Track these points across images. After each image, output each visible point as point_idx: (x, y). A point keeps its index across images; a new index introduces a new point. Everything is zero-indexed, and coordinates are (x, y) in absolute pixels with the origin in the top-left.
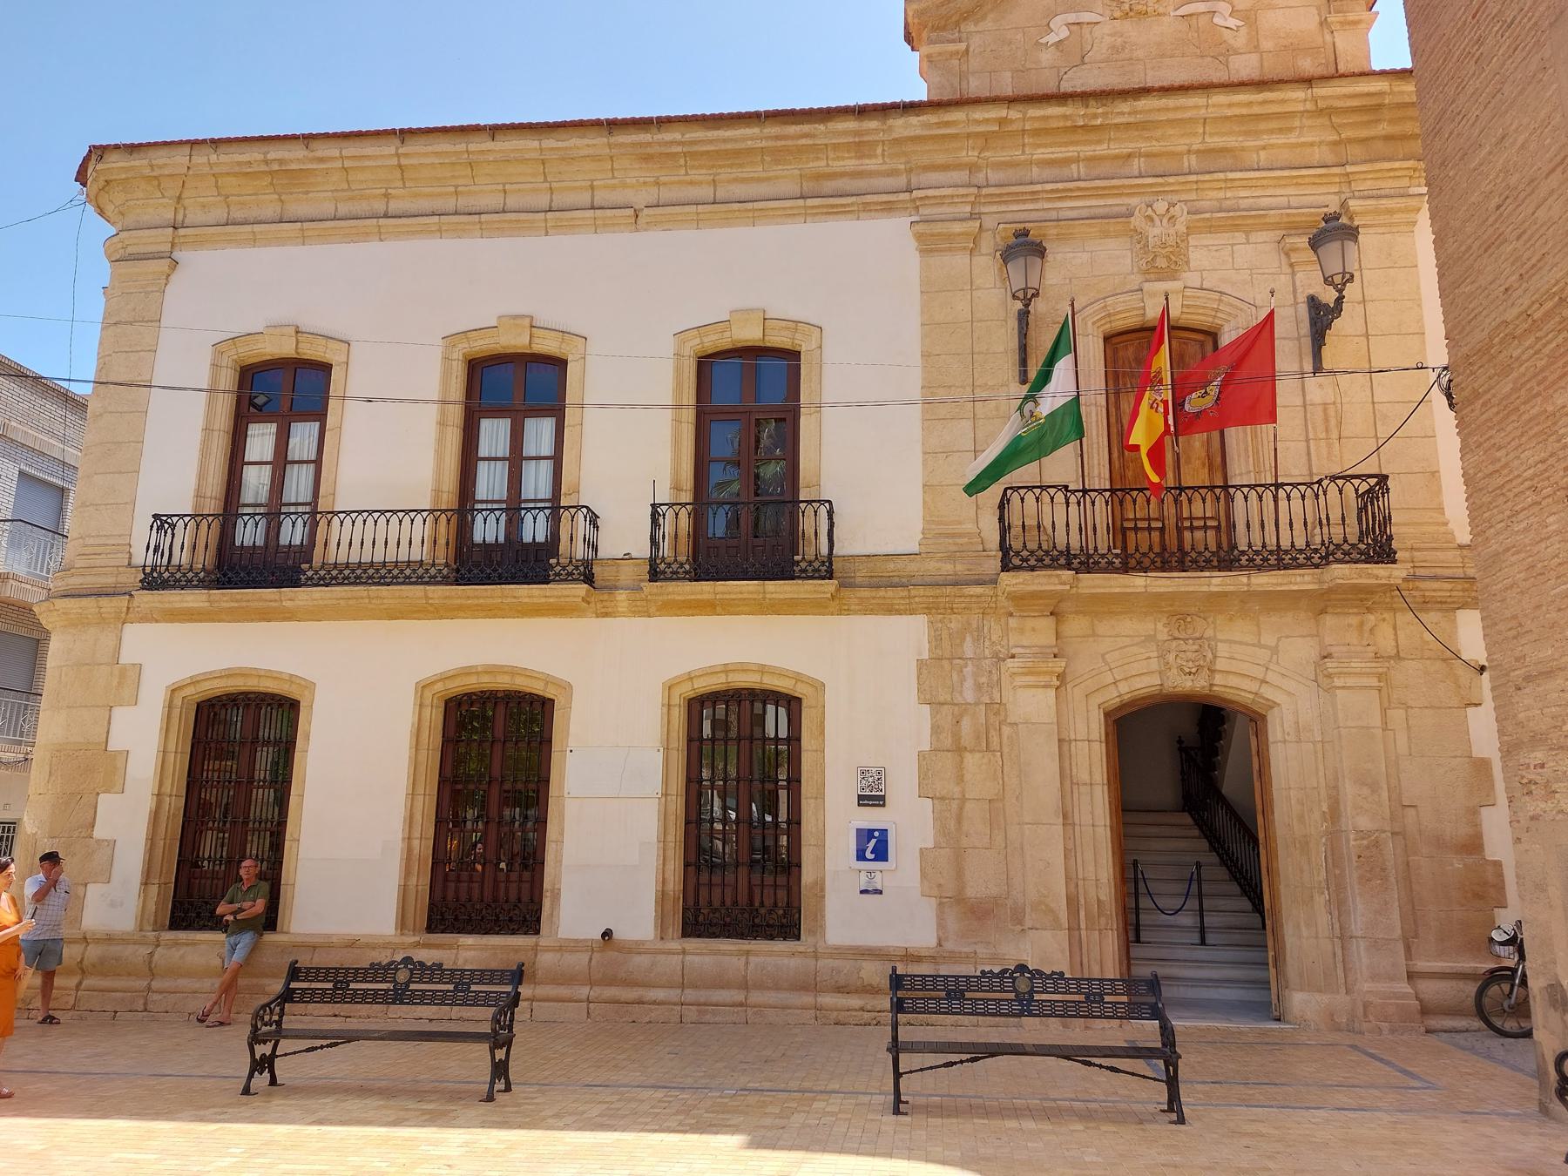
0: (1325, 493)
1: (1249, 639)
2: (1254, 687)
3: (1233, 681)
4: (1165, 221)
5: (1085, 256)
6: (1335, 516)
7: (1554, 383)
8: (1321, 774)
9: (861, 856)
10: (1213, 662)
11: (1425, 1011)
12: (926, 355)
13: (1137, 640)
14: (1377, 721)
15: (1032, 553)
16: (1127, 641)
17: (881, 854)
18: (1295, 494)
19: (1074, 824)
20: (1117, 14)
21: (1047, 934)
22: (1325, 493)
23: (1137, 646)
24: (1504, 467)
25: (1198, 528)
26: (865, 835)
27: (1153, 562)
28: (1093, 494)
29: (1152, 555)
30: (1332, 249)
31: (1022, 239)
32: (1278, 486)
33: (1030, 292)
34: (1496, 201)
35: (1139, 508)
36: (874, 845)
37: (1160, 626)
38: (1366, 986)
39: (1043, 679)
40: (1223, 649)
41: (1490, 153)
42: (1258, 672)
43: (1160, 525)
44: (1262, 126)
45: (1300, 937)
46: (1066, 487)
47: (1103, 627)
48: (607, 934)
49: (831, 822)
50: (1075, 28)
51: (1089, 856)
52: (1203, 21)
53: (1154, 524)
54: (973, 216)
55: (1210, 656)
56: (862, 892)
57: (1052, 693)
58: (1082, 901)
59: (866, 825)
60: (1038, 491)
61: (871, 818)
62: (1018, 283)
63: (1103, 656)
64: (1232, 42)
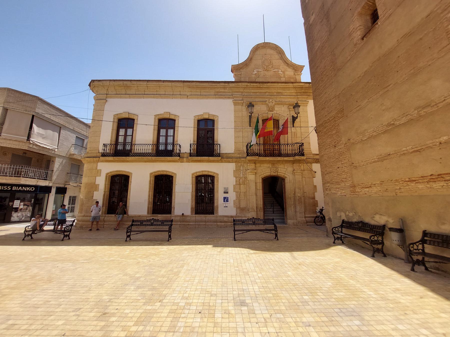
3: (281, 174)
6: (296, 149)
9: (224, 201)
11: (307, 222)
17: (227, 201)
36: (226, 199)
47: (262, 165)
48: (183, 214)
49: (219, 195)
61: (226, 195)
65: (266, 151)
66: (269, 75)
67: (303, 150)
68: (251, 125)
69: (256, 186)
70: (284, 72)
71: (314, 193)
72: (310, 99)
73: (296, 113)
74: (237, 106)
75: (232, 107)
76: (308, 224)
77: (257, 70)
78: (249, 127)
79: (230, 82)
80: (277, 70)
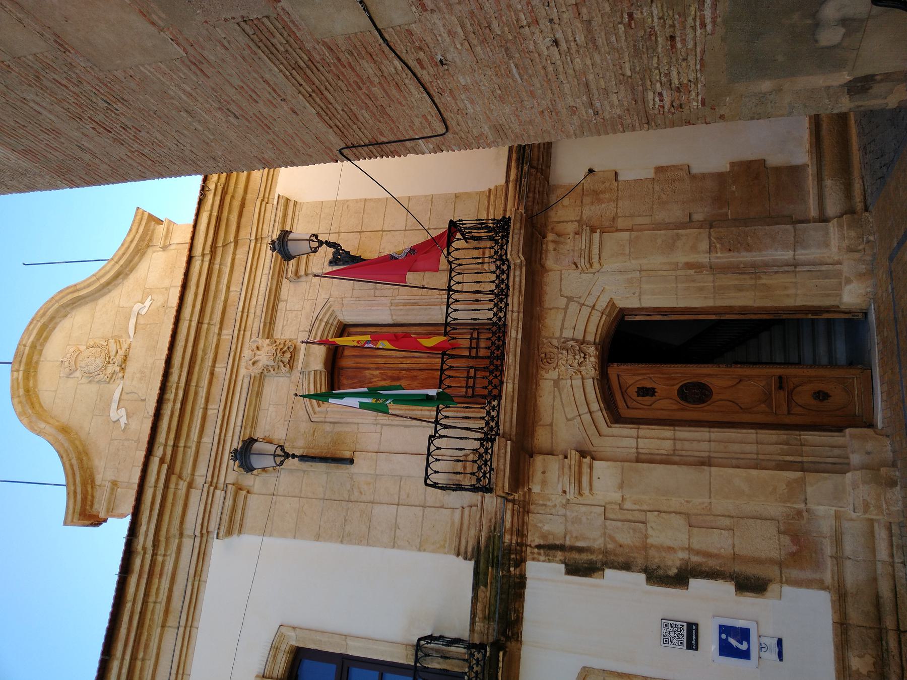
0: (458, 259)
1: (560, 317)
2: (596, 316)
3: (592, 328)
4: (258, 352)
5: (272, 409)
6: (476, 253)
7: (358, 75)
8: (665, 273)
9: (746, 655)
10: (577, 341)
11: (851, 211)
12: (318, 538)
13: (557, 394)
14: (626, 235)
15: (480, 468)
16: (558, 400)
17: (744, 634)
18: (458, 278)
19: (709, 457)
20: (121, 375)
21: (809, 490)
22: (458, 259)
23: (568, 398)
24: (426, 119)
25: (478, 343)
26: (726, 650)
27: (496, 377)
28: (440, 416)
29: (491, 377)
30: (292, 248)
31: (238, 456)
32: (449, 289)
33: (279, 452)
34: (232, 119)
35: (458, 385)
37: (547, 376)
38: (834, 249)
39: (585, 470)
40: (568, 334)
41: (199, 122)
42: (586, 311)
43: (472, 371)
44: (213, 287)
45: (796, 295)
46: (431, 437)
47: (546, 418)
50: (121, 404)
51: (736, 447)
52: (142, 321)
53: (472, 373)
54: (225, 490)
55: (571, 342)
56: (781, 660)
57: (596, 464)
58: (780, 458)
59: (714, 647)
60: (431, 459)
61: (709, 640)
62: (269, 462)
63: (568, 420)
64: (159, 304)
65: (479, 391)
66: (148, 361)
67: (481, 225)
68: (347, 455)
69: (651, 460)
70: (147, 293)
71: (693, 177)
72: (270, 183)
73: (315, 250)
74: (249, 521)
75: (246, 543)
76: (859, 206)
77: (114, 406)
78: (353, 469)
79: (203, 188)
80: (132, 322)
